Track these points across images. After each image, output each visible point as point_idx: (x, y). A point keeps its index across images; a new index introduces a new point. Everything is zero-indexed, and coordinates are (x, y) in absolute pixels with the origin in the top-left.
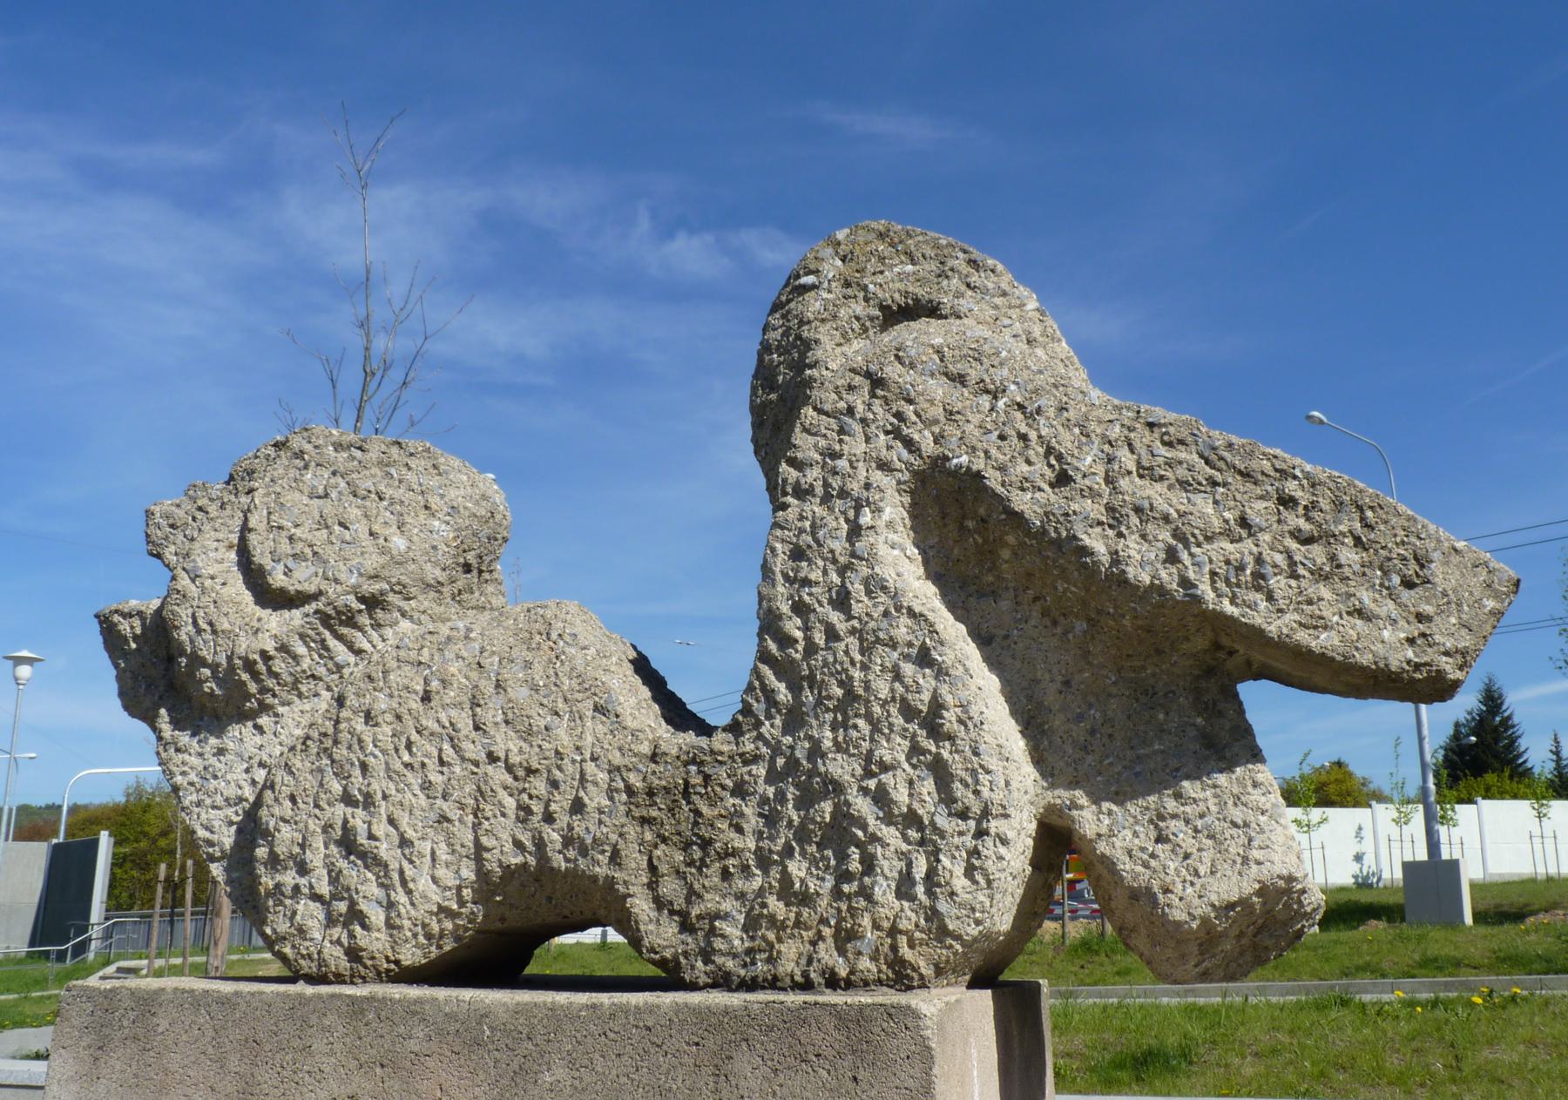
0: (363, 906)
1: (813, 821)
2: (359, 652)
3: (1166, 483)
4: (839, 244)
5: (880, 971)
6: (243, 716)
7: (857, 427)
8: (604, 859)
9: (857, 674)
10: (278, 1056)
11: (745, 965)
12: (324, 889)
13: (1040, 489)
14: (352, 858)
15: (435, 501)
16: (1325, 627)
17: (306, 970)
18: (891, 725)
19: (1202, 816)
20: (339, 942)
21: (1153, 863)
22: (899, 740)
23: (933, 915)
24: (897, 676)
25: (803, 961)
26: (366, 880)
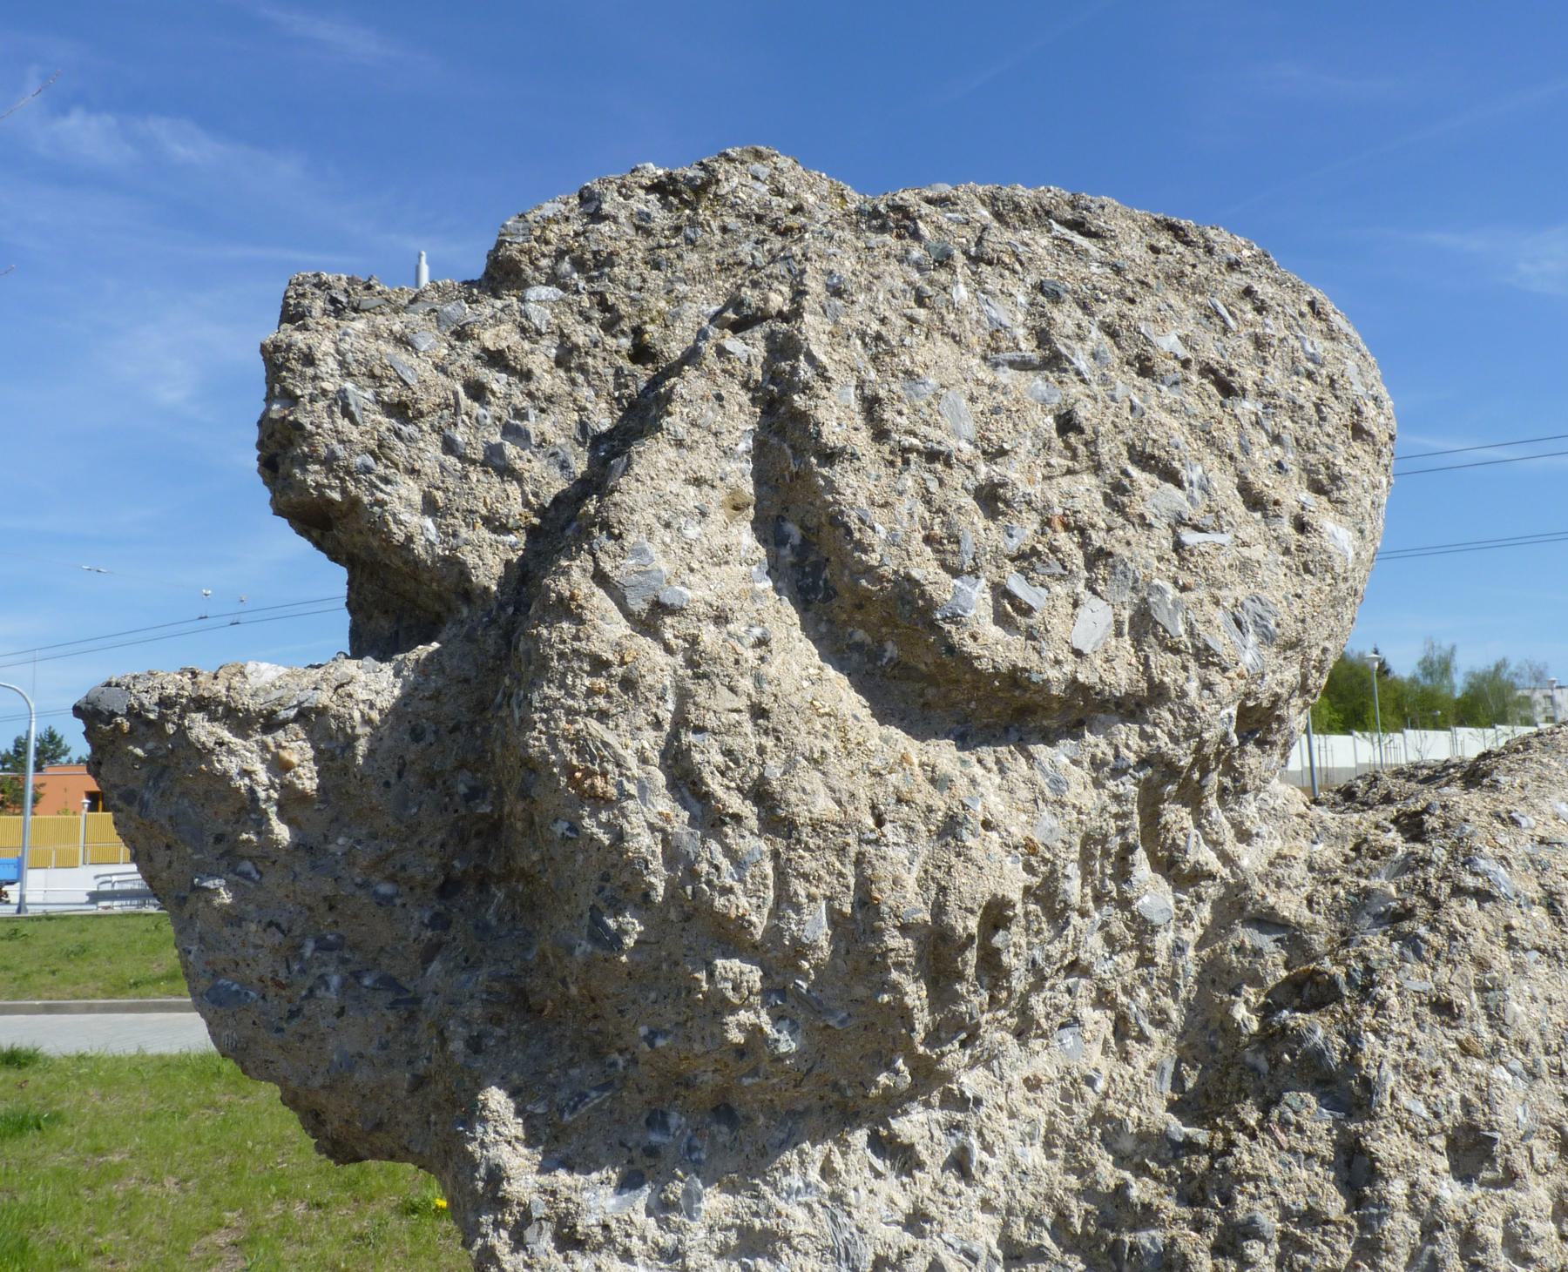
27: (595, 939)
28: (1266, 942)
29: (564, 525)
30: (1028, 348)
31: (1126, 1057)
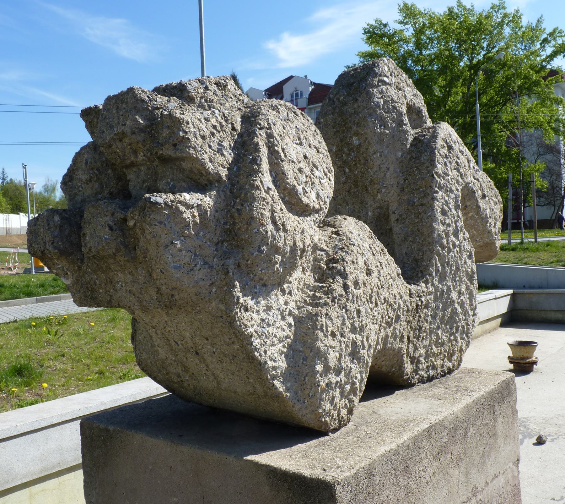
27: (258, 251)
28: (323, 253)
31: (305, 274)
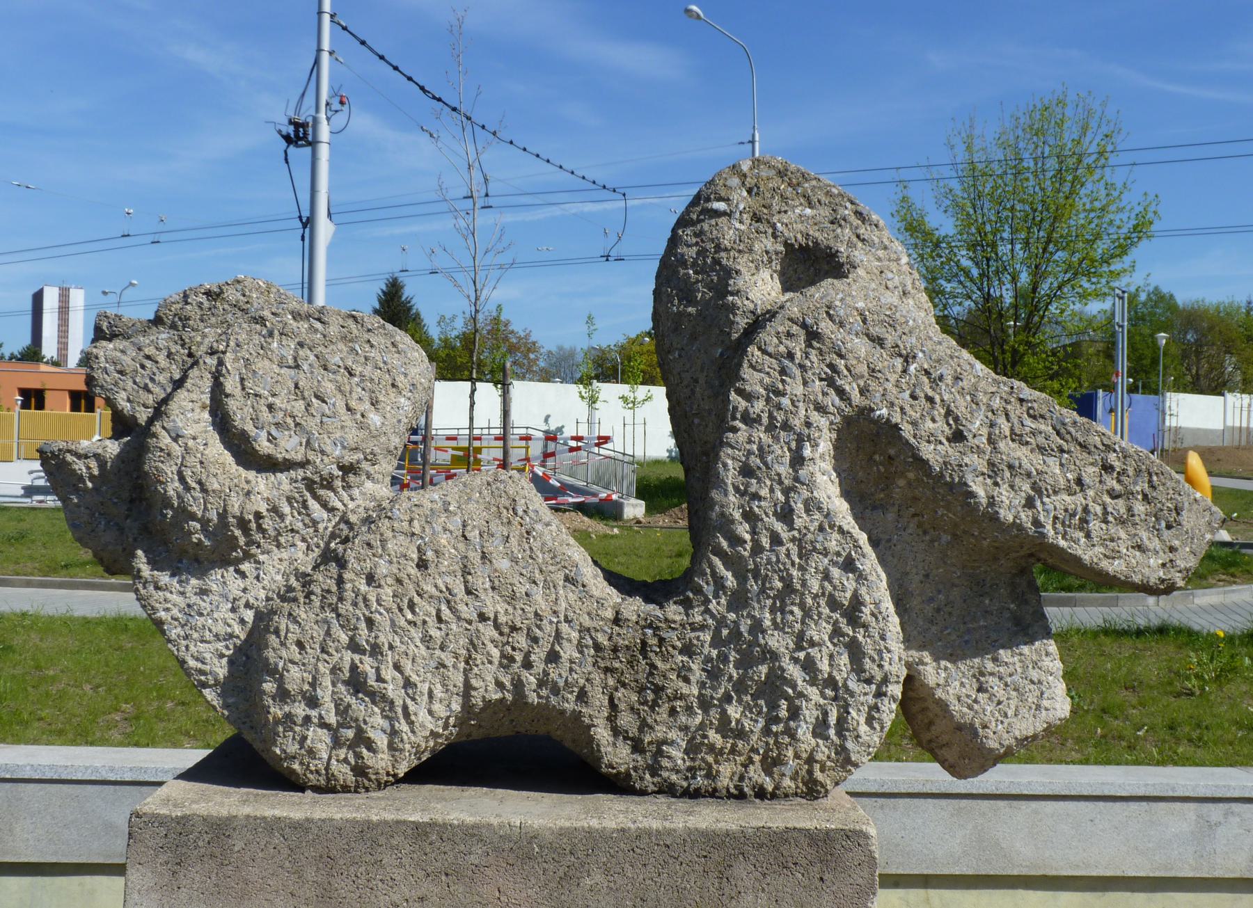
0: (371, 734)
1: (752, 679)
2: (332, 510)
3: (1030, 447)
4: (745, 176)
5: (797, 787)
6: (225, 562)
7: (797, 372)
8: (572, 697)
9: (795, 573)
10: (352, 869)
11: (686, 779)
12: (332, 719)
13: (941, 443)
14: (360, 695)
15: (400, 380)
16: (1120, 557)
17: (315, 782)
18: (819, 614)
19: (1011, 675)
20: (346, 761)
21: (976, 707)
22: (824, 624)
23: (842, 750)
24: (827, 576)
25: (736, 778)
26: (373, 713)
29: (159, 411)
30: (291, 362)
